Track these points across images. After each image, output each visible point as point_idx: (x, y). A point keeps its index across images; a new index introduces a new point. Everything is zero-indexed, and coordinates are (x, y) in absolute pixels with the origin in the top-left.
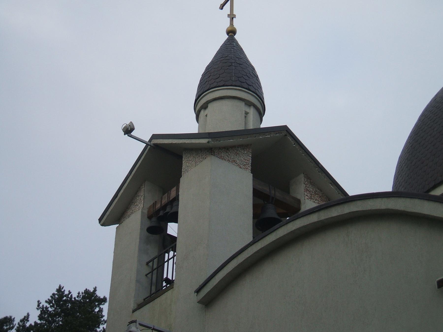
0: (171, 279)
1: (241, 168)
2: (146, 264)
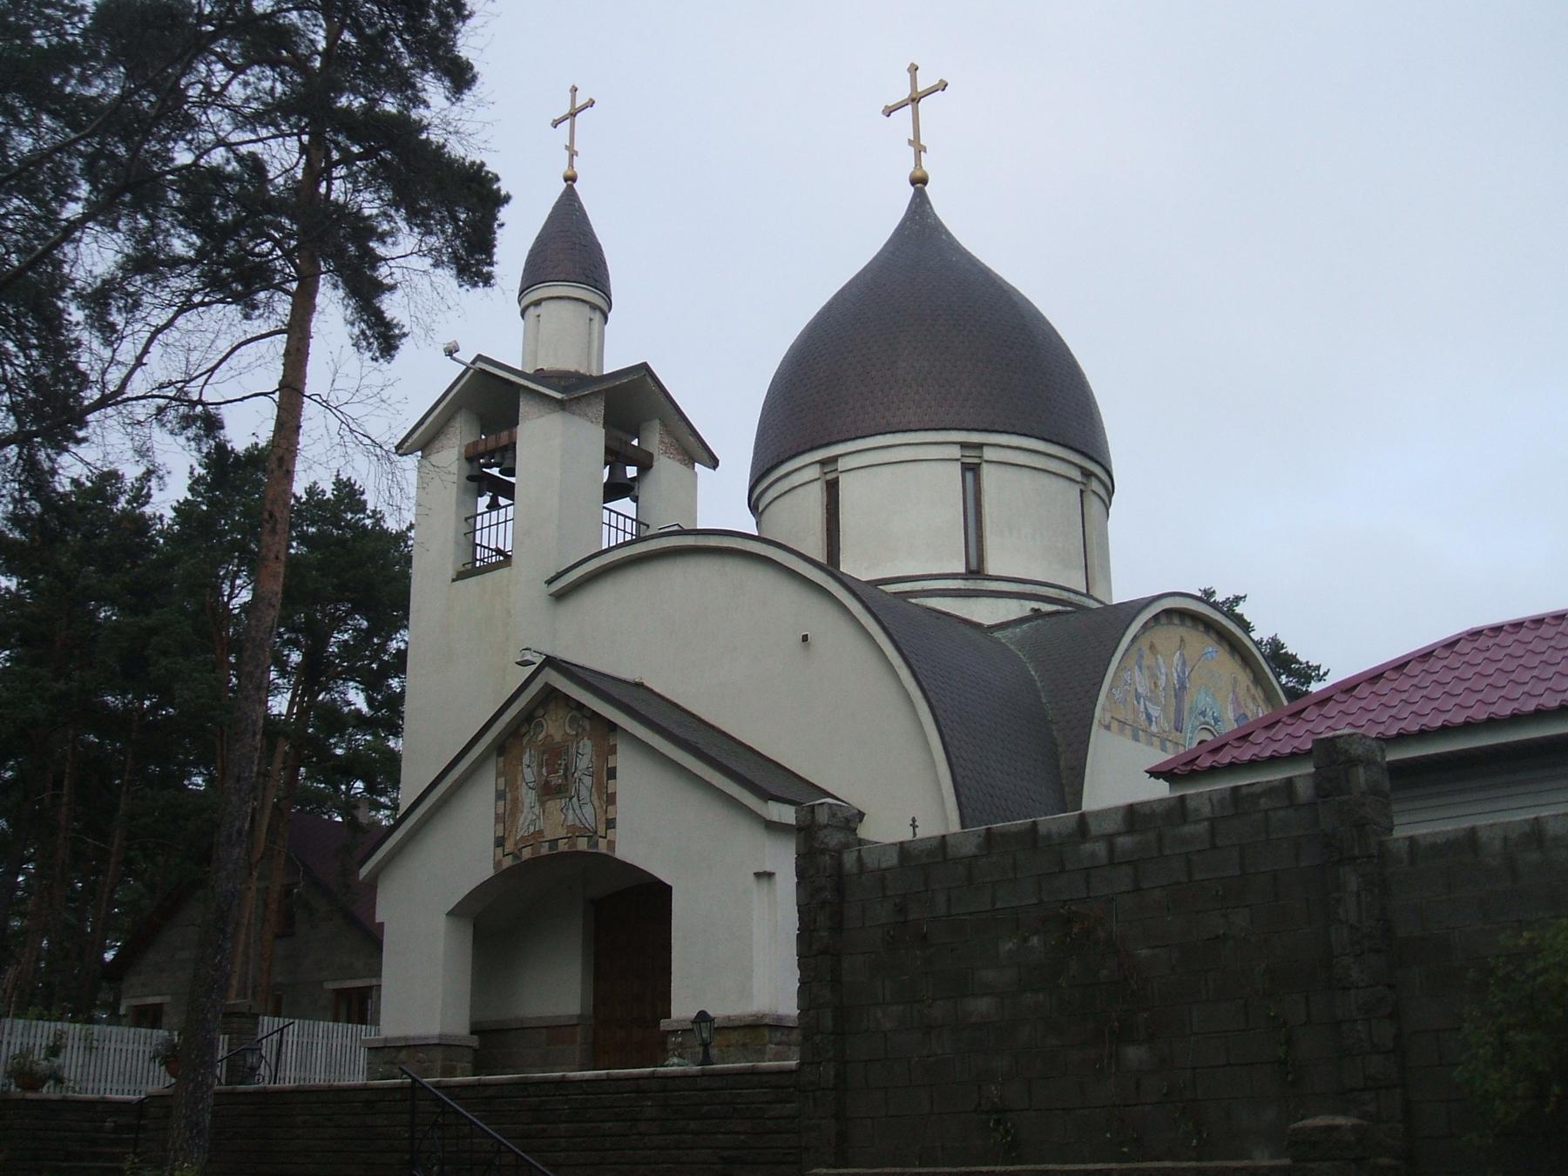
0: (503, 549)
1: (592, 422)
2: (464, 518)
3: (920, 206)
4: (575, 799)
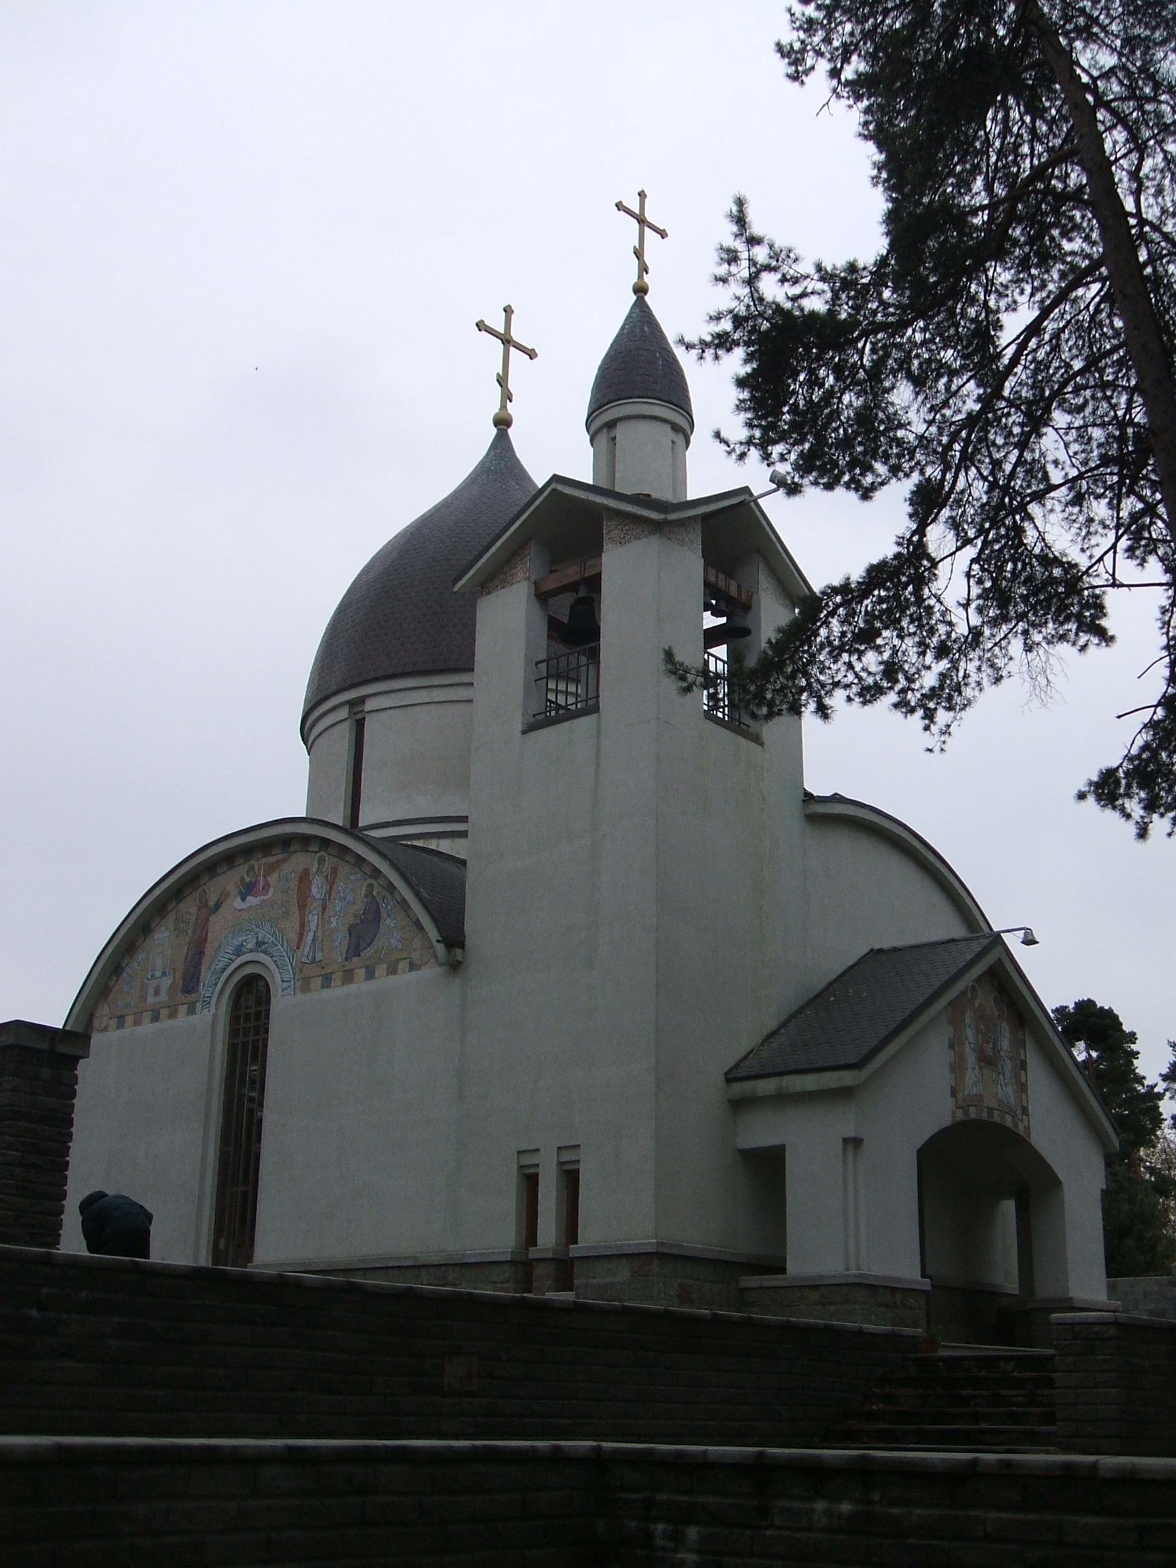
3: (502, 445)
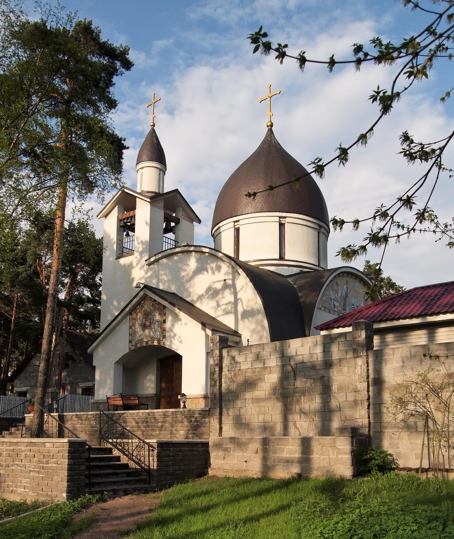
4: (153, 329)
